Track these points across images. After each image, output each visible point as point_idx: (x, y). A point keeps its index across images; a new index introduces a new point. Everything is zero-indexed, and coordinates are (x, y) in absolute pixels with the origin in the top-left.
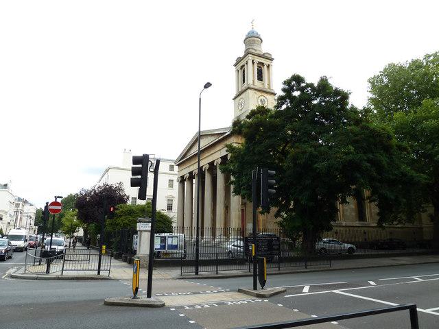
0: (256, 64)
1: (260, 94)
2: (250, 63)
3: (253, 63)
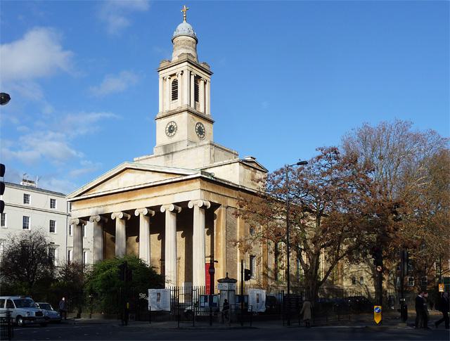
0: (193, 77)
1: (198, 120)
2: (186, 74)
3: (191, 75)
